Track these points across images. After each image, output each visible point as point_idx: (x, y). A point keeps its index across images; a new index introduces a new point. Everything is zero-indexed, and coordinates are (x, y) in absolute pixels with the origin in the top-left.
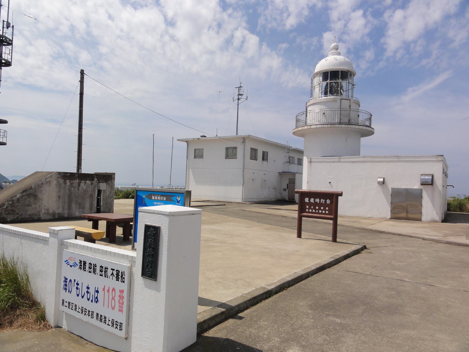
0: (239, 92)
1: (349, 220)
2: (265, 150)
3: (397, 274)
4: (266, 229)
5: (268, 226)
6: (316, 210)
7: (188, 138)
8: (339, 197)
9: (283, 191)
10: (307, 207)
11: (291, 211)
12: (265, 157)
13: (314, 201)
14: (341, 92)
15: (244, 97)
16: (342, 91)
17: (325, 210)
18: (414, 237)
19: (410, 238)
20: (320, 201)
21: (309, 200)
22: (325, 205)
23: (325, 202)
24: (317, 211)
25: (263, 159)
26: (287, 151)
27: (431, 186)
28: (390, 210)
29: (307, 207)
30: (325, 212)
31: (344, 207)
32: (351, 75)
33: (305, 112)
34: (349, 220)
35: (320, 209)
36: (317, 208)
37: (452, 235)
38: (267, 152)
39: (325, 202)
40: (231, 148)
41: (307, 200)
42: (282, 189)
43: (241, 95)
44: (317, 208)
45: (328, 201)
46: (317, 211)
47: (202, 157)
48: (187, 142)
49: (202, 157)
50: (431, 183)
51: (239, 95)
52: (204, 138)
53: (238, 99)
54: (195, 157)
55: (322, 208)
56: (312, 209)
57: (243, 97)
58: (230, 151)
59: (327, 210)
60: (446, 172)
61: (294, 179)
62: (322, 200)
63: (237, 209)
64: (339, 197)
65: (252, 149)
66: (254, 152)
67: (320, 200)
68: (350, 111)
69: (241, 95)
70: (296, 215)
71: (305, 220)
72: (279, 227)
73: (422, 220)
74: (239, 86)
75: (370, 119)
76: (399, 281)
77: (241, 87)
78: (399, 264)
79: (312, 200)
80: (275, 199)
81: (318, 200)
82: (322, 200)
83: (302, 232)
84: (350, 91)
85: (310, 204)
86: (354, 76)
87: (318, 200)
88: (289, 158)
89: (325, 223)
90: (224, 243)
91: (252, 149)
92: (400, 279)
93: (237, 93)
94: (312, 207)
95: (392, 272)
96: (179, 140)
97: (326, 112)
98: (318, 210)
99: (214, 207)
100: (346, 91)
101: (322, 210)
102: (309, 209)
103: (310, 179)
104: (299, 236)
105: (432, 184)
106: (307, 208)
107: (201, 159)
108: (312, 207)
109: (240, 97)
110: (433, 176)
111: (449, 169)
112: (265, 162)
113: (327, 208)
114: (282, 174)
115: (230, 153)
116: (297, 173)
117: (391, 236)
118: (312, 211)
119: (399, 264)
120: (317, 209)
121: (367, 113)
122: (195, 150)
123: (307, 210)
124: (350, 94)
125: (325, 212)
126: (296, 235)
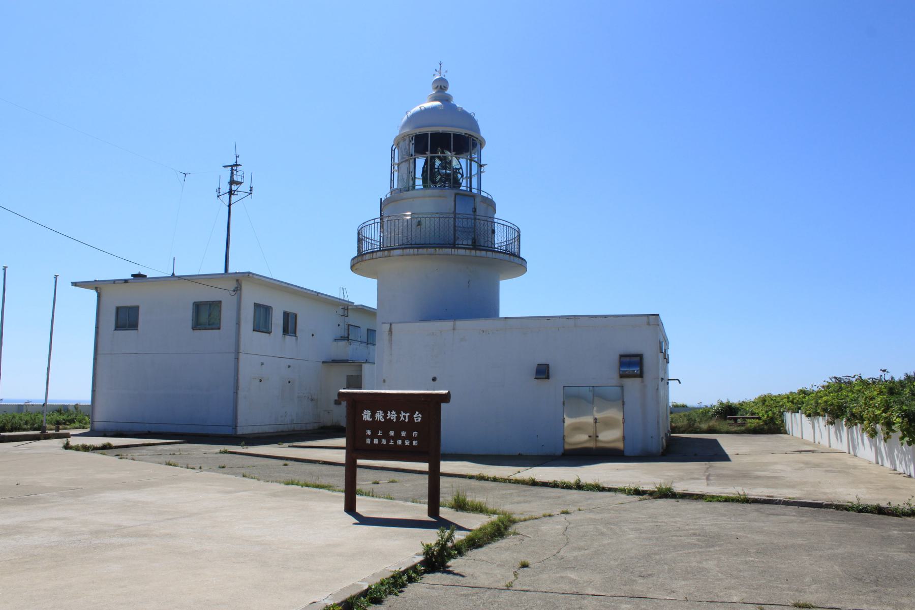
1: (598, 517)
2: (289, 310)
3: (570, 579)
4: (274, 495)
6: (388, 438)
8: (443, 405)
9: (333, 406)
10: (369, 432)
11: (334, 451)
12: (290, 325)
13: (385, 417)
15: (245, 187)
18: (610, 490)
20: (398, 418)
21: (373, 416)
22: (410, 426)
23: (411, 418)
25: (286, 331)
26: (341, 312)
27: (639, 380)
29: (369, 432)
30: (411, 443)
32: (475, 145)
34: (598, 517)
35: (398, 436)
36: (392, 433)
37: (681, 479)
38: (296, 315)
39: (411, 418)
41: (367, 416)
42: (333, 402)
44: (392, 433)
45: (418, 417)
48: (96, 289)
51: (232, 182)
53: (231, 193)
55: (403, 434)
56: (380, 439)
59: (415, 439)
62: (403, 414)
64: (443, 405)
65: (257, 306)
66: (263, 313)
67: (398, 413)
68: (475, 219)
70: (340, 456)
74: (233, 163)
76: (573, 597)
77: (237, 165)
78: (575, 553)
79: (379, 416)
80: (316, 426)
81: (392, 415)
82: (403, 414)
85: (374, 425)
86: (482, 147)
87: (392, 415)
90: (145, 536)
91: (257, 306)
92: (575, 591)
93: (228, 179)
94: (380, 433)
95: (558, 575)
96: (75, 284)
97: (423, 221)
98: (395, 438)
102: (372, 437)
103: (394, 374)
106: (368, 436)
108: (380, 433)
109: (234, 187)
110: (518, 232)
112: (289, 339)
116: (367, 362)
118: (380, 441)
119: (575, 553)
120: (392, 437)
123: (368, 441)
124: (474, 185)
125: (411, 443)
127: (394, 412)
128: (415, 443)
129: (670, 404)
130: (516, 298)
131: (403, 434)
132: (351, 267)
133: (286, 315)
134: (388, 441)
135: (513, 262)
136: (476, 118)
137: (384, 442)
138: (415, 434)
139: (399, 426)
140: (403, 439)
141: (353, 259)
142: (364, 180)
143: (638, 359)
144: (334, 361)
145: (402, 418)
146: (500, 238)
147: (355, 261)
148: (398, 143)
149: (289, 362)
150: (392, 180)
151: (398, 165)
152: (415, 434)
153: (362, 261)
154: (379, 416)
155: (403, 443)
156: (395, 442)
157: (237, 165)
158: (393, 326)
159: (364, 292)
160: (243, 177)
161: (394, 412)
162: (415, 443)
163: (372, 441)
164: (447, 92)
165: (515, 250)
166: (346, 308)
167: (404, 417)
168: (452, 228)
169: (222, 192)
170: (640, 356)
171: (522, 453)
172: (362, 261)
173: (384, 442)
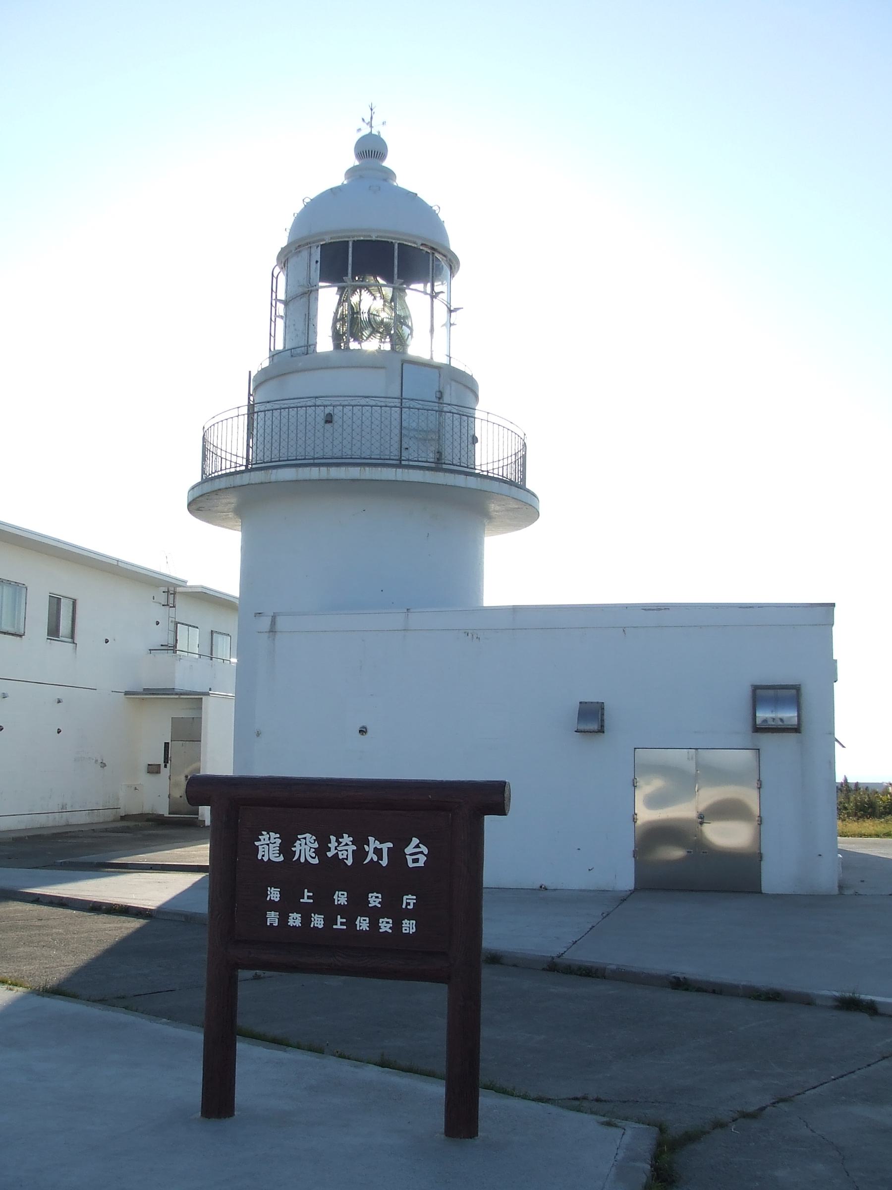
10: (274, 894)
13: (321, 851)
17: (398, 916)
20: (360, 854)
21: (286, 848)
22: (395, 879)
23: (397, 855)
24: (340, 924)
25: (53, 631)
26: (163, 598)
29: (274, 894)
30: (397, 926)
33: (245, 410)
35: (358, 906)
36: (341, 898)
39: (397, 855)
41: (268, 846)
44: (341, 898)
45: (416, 853)
55: (374, 899)
62: (373, 843)
64: (490, 822)
67: (360, 842)
80: (109, 815)
81: (343, 848)
82: (373, 843)
85: (290, 873)
87: (343, 848)
94: (307, 897)
101: (374, 915)
106: (273, 906)
108: (307, 897)
118: (306, 920)
123: (273, 918)
125: (397, 926)
126: (188, 1082)
127: (346, 839)
128: (409, 926)
129: (839, 779)
130: (514, 570)
131: (374, 899)
132: (190, 505)
133: (55, 602)
134: (330, 921)
135: (512, 498)
136: (442, 216)
137: (318, 921)
138: (409, 900)
139: (361, 877)
140: (374, 915)
141: (193, 488)
142: (210, 341)
143: (794, 692)
144: (148, 691)
145: (372, 856)
146: (490, 455)
147: (197, 493)
148: (285, 258)
149: (60, 692)
150: (272, 336)
151: (286, 303)
152: (409, 900)
153: (205, 500)
154: (305, 848)
155: (374, 925)
156: (351, 923)
158: (279, 620)
159: (213, 558)
161: (346, 839)
162: (409, 926)
163: (283, 919)
164: (386, 164)
165: (518, 481)
166: (170, 592)
167: (378, 852)
168: (397, 431)
170: (797, 688)
171: (547, 883)
172: (205, 500)
173: (318, 921)
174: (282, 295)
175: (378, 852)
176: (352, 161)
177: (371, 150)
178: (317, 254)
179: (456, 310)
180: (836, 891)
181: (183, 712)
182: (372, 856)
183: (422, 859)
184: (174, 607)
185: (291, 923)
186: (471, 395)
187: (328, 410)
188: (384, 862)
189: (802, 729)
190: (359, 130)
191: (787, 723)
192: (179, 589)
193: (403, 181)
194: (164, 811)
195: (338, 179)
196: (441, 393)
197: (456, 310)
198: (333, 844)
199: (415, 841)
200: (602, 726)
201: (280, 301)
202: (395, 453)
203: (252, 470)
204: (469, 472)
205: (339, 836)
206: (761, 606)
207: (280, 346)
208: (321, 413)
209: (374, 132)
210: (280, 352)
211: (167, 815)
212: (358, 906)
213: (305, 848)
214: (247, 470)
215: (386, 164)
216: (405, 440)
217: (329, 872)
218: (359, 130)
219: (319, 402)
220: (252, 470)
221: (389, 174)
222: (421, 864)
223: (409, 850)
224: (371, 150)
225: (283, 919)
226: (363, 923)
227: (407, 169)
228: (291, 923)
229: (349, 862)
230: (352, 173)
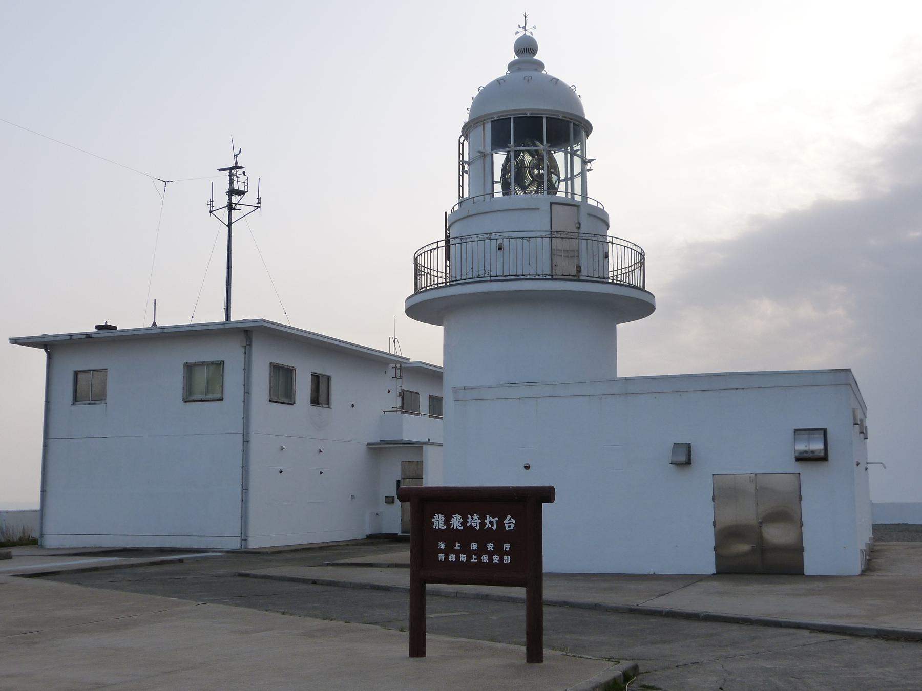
0: (231, 182)
2: (319, 371)
5: (317, 623)
7: (181, 385)
10: (442, 545)
12: (320, 394)
13: (464, 523)
14: (550, 180)
16: (554, 178)
17: (502, 554)
19: (771, 631)
20: (482, 524)
21: (447, 522)
22: (500, 536)
23: (500, 524)
24: (474, 559)
25: (315, 401)
28: (712, 543)
29: (442, 545)
30: (501, 559)
31: (567, 543)
33: (443, 244)
35: (482, 550)
36: (474, 546)
38: (328, 378)
39: (500, 524)
40: (203, 364)
41: (438, 522)
43: (241, 193)
44: (474, 546)
45: (510, 523)
46: (474, 559)
47: (100, 398)
49: (100, 398)
50: (822, 454)
51: (232, 192)
52: (107, 333)
53: (230, 207)
54: (76, 400)
55: (490, 547)
57: (245, 199)
58: (201, 377)
59: (507, 553)
60: (862, 421)
61: (420, 463)
62: (489, 518)
63: (222, 571)
67: (483, 518)
69: (241, 193)
70: (403, 579)
71: (438, 594)
72: (357, 625)
73: (808, 571)
74: (232, 164)
75: (642, 264)
77: (237, 167)
81: (474, 521)
82: (489, 518)
83: (428, 636)
84: (578, 181)
85: (449, 535)
87: (474, 521)
88: (402, 394)
89: (457, 595)
93: (227, 188)
99: (140, 570)
100: (566, 180)
101: (490, 554)
102: (447, 553)
104: (417, 649)
105: (825, 458)
106: (441, 551)
107: (97, 408)
109: (235, 199)
111: (869, 414)
113: (507, 546)
114: (379, 449)
115: (202, 384)
117: (718, 628)
118: (458, 558)
121: (630, 247)
122: (76, 373)
123: (441, 557)
125: (501, 559)
126: (406, 648)
127: (476, 517)
131: (490, 547)
137: (463, 558)
139: (483, 535)
140: (490, 554)
145: (488, 525)
148: (467, 130)
150: (461, 186)
152: (507, 546)
154: (456, 522)
155: (490, 559)
156: (479, 558)
157: (237, 167)
159: (425, 344)
160: (246, 184)
161: (476, 517)
163: (447, 557)
164: (536, 57)
167: (491, 523)
169: (216, 205)
173: (463, 558)
174: (466, 158)
175: (491, 523)
176: (512, 57)
177: (526, 48)
178: (489, 127)
179: (590, 161)
180: (855, 566)
181: (413, 458)
182: (488, 525)
183: (513, 526)
184: (401, 378)
185: (450, 559)
186: (605, 226)
187: (500, 241)
188: (494, 528)
189: (829, 458)
190: (517, 33)
191: (817, 454)
192: (403, 365)
193: (550, 70)
194: (398, 531)
195: (502, 71)
196: (579, 224)
197: (590, 161)
198: (469, 519)
199: (509, 517)
200: (690, 459)
201: (466, 162)
202: (547, 271)
203: (450, 286)
204: (604, 280)
205: (472, 515)
206: (24, 512)
207: (466, 195)
208: (494, 244)
209: (528, 34)
210: (467, 199)
211: (400, 533)
212: (482, 550)
213: (456, 522)
214: (446, 286)
215: (536, 57)
216: (556, 259)
217: (468, 533)
218: (517, 33)
219: (493, 236)
220: (450, 286)
221: (541, 66)
222: (512, 528)
223: (505, 522)
224: (526, 48)
225: (447, 557)
226: (485, 559)
227: (555, 62)
228: (450, 559)
229: (478, 528)
230: (511, 66)
